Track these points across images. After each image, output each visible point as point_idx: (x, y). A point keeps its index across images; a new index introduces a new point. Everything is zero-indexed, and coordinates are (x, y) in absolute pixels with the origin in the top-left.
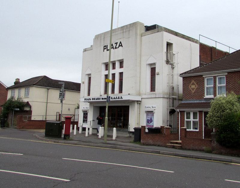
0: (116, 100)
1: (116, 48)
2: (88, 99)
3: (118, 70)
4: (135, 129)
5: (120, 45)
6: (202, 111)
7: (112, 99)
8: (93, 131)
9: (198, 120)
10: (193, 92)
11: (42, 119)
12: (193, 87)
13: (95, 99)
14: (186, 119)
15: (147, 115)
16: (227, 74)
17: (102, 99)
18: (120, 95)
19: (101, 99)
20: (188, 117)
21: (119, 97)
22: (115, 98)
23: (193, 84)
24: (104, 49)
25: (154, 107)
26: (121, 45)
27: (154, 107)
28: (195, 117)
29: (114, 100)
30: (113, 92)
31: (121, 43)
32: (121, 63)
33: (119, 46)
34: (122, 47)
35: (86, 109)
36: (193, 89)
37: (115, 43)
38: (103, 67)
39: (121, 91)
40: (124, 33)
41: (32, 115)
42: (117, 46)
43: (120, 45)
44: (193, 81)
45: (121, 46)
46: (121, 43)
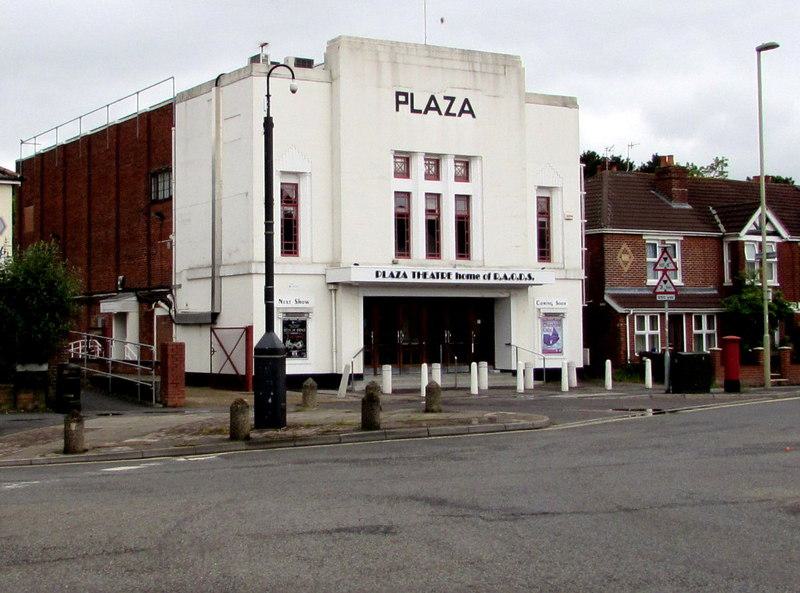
0: (511, 282)
1: (448, 113)
2: (432, 274)
3: (449, 187)
4: (181, 347)
5: (467, 108)
6: (691, 314)
7: (495, 278)
8: (393, 382)
9: (658, 332)
10: (626, 269)
11: (207, 371)
12: (625, 258)
13: (428, 276)
14: (637, 332)
15: (544, 322)
16: (682, 238)
17: (458, 276)
18: (434, 266)
19: (453, 276)
20: (641, 327)
21: (521, 275)
22: (509, 276)
23: (625, 252)
24: (398, 103)
25: (561, 304)
26: (467, 109)
27: (561, 304)
28: (653, 326)
29: (504, 282)
30: (434, 248)
31: (466, 101)
32: (465, 164)
33: (462, 111)
34: (474, 116)
35: (293, 304)
36: (626, 263)
37: (446, 98)
38: (390, 165)
39: (463, 248)
40: (478, 75)
41: (542, 367)
42: (455, 109)
43: (433, 105)
44: (624, 246)
45: (433, 109)
46: (466, 101)
